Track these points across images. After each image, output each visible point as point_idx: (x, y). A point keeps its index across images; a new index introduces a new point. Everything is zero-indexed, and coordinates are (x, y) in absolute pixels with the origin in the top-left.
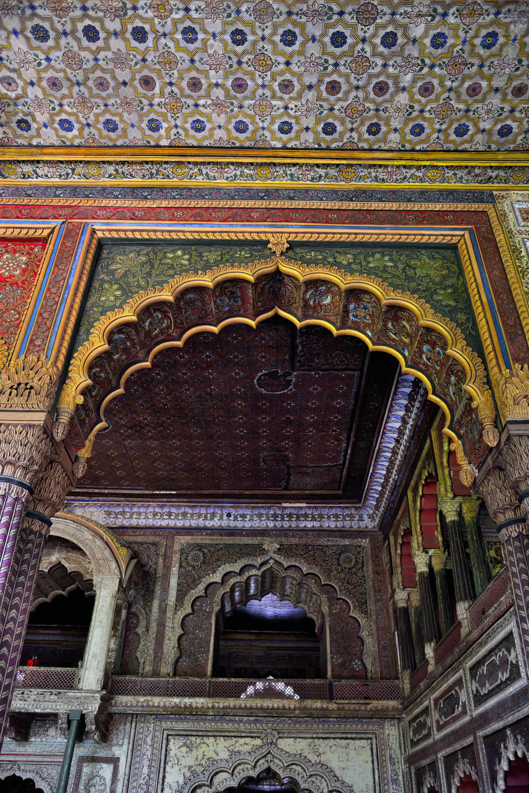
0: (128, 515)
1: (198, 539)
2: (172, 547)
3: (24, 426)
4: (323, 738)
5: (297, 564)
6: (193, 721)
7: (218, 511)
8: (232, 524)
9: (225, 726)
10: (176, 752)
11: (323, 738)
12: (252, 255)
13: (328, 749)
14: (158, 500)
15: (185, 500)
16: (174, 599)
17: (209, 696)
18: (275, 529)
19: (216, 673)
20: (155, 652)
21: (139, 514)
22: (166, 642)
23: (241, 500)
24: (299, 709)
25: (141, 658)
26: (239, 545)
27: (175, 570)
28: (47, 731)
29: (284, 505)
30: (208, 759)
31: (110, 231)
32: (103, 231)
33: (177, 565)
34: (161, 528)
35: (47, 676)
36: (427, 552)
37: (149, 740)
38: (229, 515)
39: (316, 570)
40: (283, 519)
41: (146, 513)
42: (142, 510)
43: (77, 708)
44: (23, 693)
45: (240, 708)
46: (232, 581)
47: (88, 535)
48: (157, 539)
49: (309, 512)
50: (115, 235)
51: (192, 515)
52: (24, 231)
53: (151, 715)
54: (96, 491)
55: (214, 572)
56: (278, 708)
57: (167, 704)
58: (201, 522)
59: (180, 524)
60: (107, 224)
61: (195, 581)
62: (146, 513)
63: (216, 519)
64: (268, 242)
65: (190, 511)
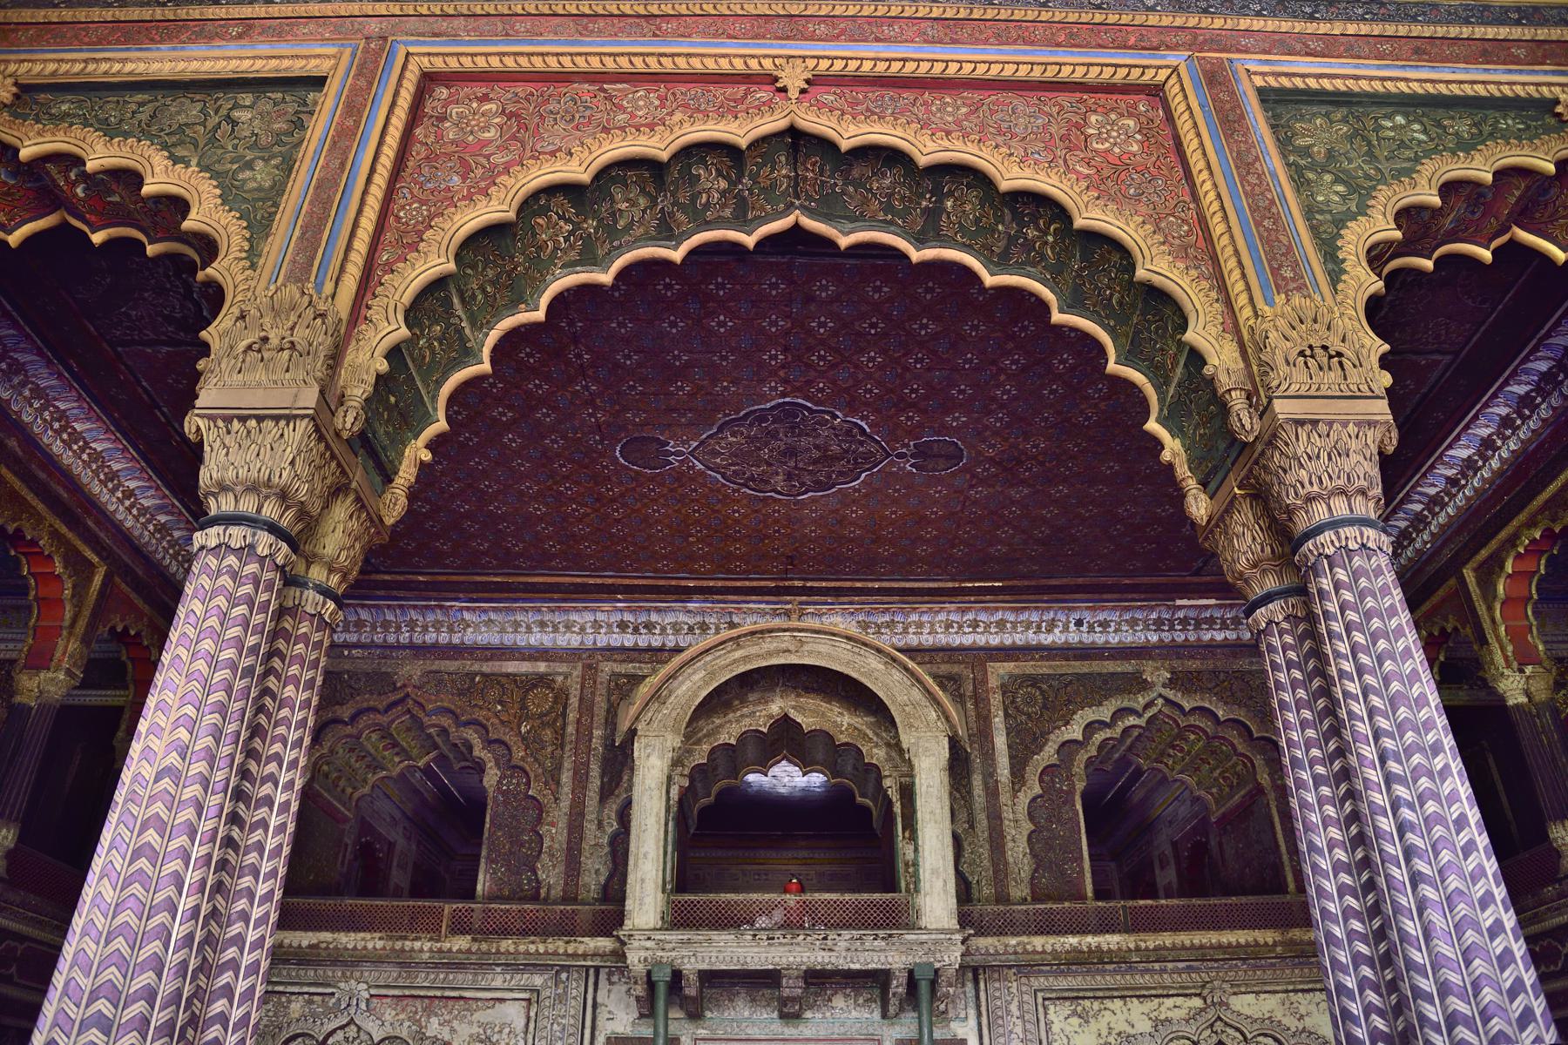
0: (899, 629)
1: (1029, 667)
2: (985, 681)
3: (1358, 424)
4: (1303, 991)
5: (1207, 705)
6: (1084, 974)
7: (1061, 617)
8: (1087, 639)
9: (1139, 980)
10: (1062, 1025)
11: (1303, 991)
12: (1528, 127)
13: (1313, 1007)
14: (959, 599)
15: (1007, 598)
16: (1006, 772)
17: (1127, 930)
18: (1161, 645)
19: (1099, 895)
20: (995, 864)
21: (920, 625)
22: (1010, 845)
23: (1105, 596)
24: (1282, 943)
25: (972, 874)
26: (1100, 674)
27: (998, 721)
28: (830, 1000)
29: (1179, 602)
30: (1119, 1034)
31: (1277, 75)
32: (1263, 74)
33: (1001, 713)
34: (961, 649)
35: (858, 908)
36: (1521, 671)
37: (1014, 1008)
38: (1079, 623)
39: (1240, 714)
40: (1172, 628)
41: (932, 625)
42: (925, 618)
43: (924, 959)
44: (825, 938)
45: (1184, 948)
46: (1099, 737)
47: (875, 663)
48: (956, 669)
49: (1217, 614)
50: (1285, 82)
51: (1014, 625)
52: (1122, 72)
53: (1010, 967)
54: (858, 585)
55: (1067, 723)
56: (1248, 945)
57: (1058, 947)
58: (1031, 637)
59: (995, 641)
60: (1267, 62)
61: (1035, 739)
62: (932, 625)
63: (1056, 631)
64: (1557, 102)
65: (1012, 619)
